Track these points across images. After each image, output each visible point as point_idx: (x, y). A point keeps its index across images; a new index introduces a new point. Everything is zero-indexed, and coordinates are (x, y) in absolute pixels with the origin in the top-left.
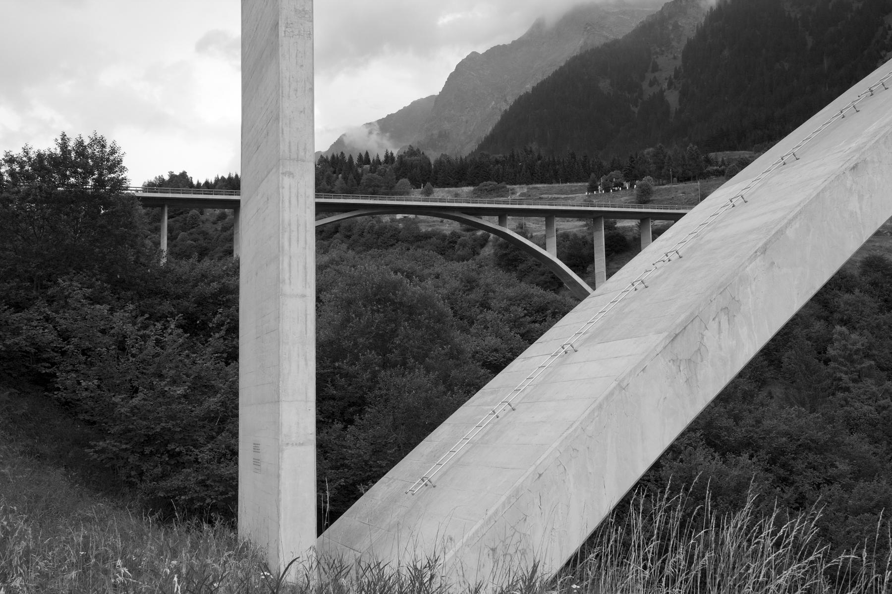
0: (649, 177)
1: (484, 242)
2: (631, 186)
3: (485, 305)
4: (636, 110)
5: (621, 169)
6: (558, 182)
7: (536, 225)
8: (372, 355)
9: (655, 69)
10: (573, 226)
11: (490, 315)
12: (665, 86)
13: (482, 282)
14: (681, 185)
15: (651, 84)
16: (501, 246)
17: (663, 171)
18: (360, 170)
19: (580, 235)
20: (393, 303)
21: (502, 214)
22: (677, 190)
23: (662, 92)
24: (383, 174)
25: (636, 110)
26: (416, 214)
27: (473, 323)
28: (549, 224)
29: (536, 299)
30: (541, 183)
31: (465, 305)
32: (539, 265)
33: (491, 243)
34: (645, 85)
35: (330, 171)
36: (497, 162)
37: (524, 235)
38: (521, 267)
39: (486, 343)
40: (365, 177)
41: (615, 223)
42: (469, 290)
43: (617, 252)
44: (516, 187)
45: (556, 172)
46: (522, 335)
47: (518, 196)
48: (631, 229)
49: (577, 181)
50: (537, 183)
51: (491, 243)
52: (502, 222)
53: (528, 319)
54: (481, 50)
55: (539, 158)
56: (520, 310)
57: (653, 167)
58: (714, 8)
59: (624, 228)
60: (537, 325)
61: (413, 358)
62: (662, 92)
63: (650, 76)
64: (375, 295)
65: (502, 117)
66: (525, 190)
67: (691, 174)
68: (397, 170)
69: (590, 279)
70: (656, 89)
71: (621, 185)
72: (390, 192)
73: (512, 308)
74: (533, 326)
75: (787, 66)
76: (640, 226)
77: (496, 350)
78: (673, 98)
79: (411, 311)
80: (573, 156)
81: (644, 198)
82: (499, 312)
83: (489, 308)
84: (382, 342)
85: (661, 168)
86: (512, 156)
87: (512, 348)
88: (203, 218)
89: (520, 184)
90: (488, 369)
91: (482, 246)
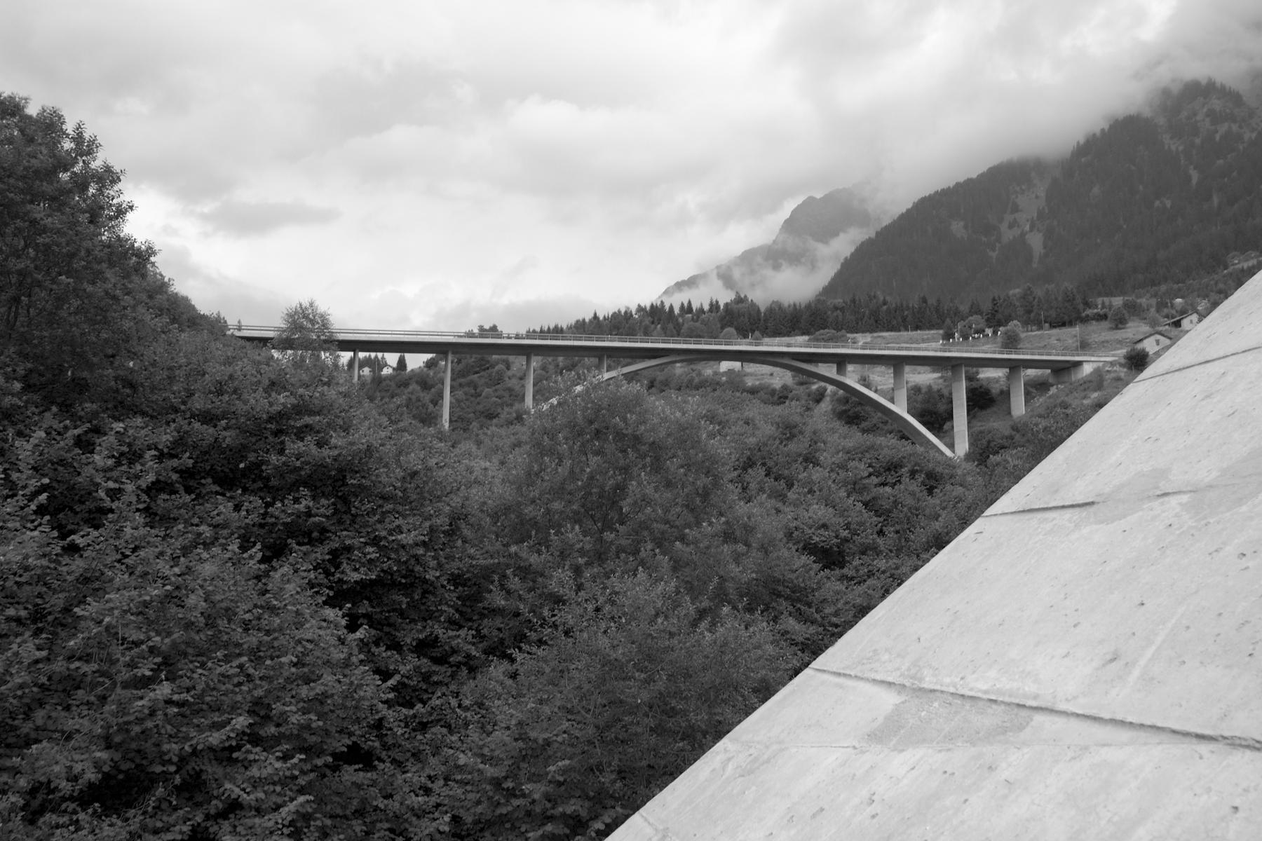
0: (1015, 322)
1: (819, 397)
2: (995, 333)
3: (810, 460)
4: (994, 255)
5: (981, 314)
6: (907, 330)
7: (882, 377)
8: (573, 534)
9: (1016, 209)
10: (925, 377)
11: (817, 474)
12: (1027, 228)
13: (808, 430)
14: (1055, 331)
15: (1011, 227)
16: (839, 401)
17: (1032, 315)
18: (680, 320)
19: (935, 388)
20: (620, 436)
21: (841, 361)
22: (1050, 337)
23: (1023, 235)
24: (705, 323)
25: (994, 255)
26: (742, 361)
27: (793, 485)
28: (898, 373)
29: (886, 451)
30: (888, 331)
31: (781, 459)
32: (885, 423)
33: (828, 399)
34: (1004, 227)
35: (647, 321)
36: (836, 308)
37: (868, 386)
38: (864, 425)
39: (811, 514)
40: (686, 326)
41: (978, 373)
42: (788, 439)
43: (983, 407)
44: (858, 336)
45: (904, 320)
46: (866, 504)
47: (860, 344)
48: (997, 380)
49: (930, 328)
50: (881, 331)
51: (828, 399)
52: (841, 370)
53: (875, 480)
54: (818, 196)
55: (885, 303)
56: (862, 466)
57: (1020, 311)
58: (1082, 142)
59: (988, 379)
60: (888, 489)
61: (653, 540)
62: (1023, 235)
63: (1009, 218)
64: (591, 422)
65: (843, 265)
66: (869, 339)
67: (1066, 318)
68: (722, 319)
69: (947, 440)
70: (1016, 232)
71: (982, 331)
72: (713, 336)
73: (852, 464)
74: (881, 490)
75: (1168, 204)
76: (1008, 378)
77: (825, 526)
78: (1036, 242)
79: (656, 455)
80: (924, 300)
81: (1011, 342)
82: (832, 470)
83: (816, 463)
84: (602, 508)
85: (1029, 312)
86: (854, 301)
87: (849, 523)
88: (509, 373)
89: (863, 332)
90: (810, 554)
91: (818, 401)
